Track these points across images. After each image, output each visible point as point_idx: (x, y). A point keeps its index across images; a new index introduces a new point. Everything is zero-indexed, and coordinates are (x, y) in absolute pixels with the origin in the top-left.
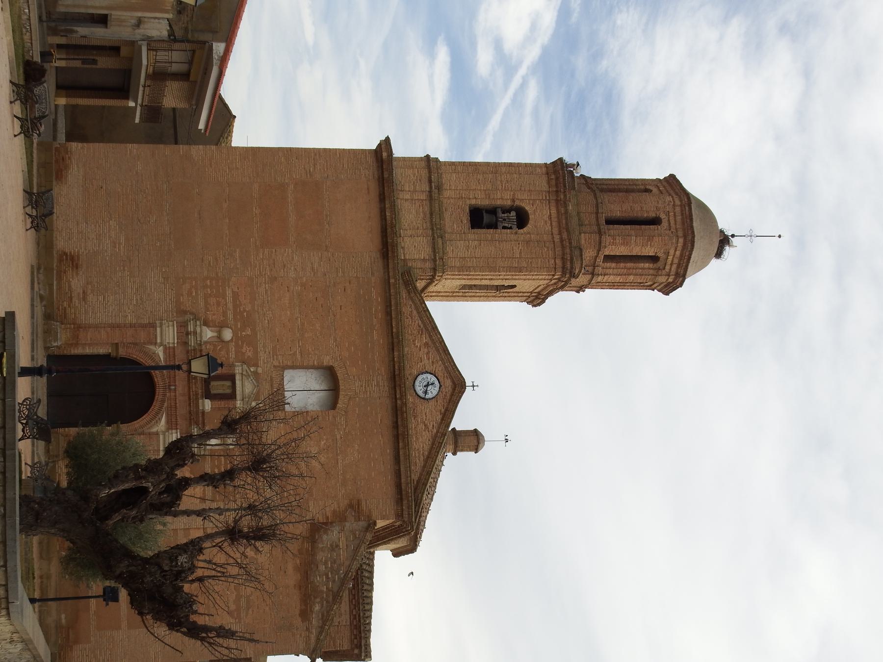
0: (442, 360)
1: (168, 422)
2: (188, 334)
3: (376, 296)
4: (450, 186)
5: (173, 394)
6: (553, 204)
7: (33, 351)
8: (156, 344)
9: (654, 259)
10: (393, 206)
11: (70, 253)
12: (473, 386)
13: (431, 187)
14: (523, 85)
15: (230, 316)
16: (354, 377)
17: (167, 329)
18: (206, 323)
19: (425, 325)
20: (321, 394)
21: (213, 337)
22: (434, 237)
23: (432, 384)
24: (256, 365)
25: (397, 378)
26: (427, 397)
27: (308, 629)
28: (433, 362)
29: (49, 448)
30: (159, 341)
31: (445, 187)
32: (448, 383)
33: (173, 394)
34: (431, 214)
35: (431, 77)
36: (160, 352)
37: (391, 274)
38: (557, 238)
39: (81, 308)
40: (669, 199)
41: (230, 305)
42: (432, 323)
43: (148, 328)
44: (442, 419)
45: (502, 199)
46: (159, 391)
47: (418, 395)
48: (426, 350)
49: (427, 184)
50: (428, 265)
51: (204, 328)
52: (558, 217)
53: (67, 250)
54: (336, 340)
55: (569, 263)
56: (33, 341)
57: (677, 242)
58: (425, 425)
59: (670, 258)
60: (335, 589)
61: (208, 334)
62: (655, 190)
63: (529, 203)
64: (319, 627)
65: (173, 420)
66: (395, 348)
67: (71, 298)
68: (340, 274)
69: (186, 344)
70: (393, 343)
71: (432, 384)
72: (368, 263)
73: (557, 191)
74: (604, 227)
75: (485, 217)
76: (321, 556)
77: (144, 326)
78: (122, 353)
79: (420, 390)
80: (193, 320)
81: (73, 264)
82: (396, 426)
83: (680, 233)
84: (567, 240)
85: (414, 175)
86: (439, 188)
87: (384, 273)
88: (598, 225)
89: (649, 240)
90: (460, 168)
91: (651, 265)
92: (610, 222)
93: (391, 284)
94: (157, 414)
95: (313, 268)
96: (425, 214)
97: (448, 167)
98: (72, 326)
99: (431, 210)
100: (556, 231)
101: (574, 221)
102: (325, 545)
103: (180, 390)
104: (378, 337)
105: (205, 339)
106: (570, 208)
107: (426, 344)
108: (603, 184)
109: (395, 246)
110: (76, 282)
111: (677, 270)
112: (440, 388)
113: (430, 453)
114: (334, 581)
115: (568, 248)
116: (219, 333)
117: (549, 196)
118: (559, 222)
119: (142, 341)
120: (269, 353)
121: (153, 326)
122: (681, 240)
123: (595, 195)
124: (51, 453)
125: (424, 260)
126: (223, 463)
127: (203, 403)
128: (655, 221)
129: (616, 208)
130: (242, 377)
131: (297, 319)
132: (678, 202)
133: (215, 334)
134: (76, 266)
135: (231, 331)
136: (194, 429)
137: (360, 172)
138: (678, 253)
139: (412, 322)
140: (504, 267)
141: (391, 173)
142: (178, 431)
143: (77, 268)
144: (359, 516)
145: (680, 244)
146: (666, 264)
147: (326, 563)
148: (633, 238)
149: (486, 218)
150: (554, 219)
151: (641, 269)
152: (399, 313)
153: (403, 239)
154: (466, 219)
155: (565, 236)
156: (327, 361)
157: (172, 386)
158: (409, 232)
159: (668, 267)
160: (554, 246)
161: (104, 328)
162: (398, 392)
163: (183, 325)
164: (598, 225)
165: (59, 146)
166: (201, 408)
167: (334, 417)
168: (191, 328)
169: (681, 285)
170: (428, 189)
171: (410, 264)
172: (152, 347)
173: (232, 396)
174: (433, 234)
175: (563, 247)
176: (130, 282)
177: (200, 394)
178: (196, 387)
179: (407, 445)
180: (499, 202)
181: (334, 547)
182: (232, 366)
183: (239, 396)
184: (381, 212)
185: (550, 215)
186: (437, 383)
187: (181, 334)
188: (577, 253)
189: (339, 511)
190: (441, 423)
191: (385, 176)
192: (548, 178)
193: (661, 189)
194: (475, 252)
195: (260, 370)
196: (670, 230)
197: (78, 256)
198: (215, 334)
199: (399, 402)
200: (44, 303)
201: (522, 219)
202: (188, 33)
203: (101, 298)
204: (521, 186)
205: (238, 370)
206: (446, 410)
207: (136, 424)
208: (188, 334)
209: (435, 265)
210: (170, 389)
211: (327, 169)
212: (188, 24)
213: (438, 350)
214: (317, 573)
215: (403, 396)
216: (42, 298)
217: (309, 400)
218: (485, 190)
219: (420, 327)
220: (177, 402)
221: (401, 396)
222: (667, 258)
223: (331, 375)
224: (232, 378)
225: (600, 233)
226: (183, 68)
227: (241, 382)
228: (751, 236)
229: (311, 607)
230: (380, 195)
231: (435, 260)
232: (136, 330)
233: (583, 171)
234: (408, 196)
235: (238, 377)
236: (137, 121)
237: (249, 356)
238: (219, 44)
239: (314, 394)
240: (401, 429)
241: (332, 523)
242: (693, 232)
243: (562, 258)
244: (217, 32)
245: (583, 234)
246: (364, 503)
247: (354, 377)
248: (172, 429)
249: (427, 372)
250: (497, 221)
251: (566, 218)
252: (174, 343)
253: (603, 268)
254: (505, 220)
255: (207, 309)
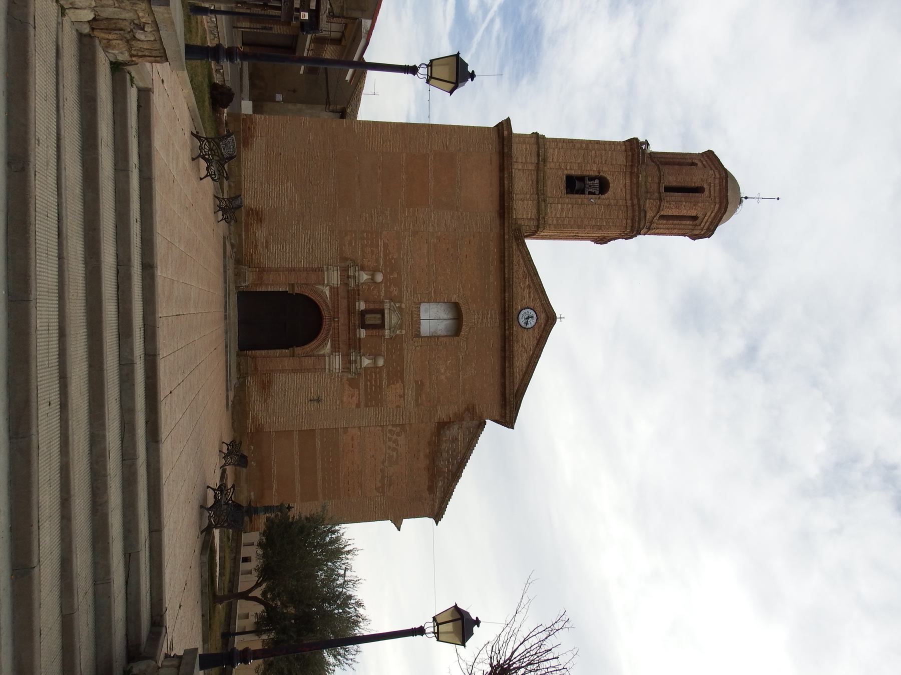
0: (539, 298)
1: (333, 346)
2: (348, 277)
3: (493, 247)
4: (553, 158)
5: (336, 324)
6: (628, 175)
7: (226, 311)
8: (323, 284)
9: (695, 218)
10: (511, 177)
11: (256, 208)
12: (561, 318)
13: (538, 160)
14: (492, 21)
15: (381, 262)
16: (474, 312)
17: (333, 272)
18: (363, 268)
19: (528, 271)
20: (448, 322)
21: (368, 279)
22: (539, 201)
23: (532, 317)
24: (401, 302)
25: (507, 314)
26: (528, 327)
27: (433, 499)
28: (532, 300)
29: (240, 368)
30: (326, 282)
31: (548, 160)
32: (543, 316)
33: (336, 324)
34: (537, 182)
35: (444, 11)
36: (327, 291)
37: (506, 231)
38: (629, 202)
39: (264, 255)
40: (711, 172)
41: (381, 254)
42: (531, 262)
43: (317, 272)
44: (537, 344)
45: (591, 170)
46: (326, 321)
47: (521, 326)
48: (528, 291)
49: (536, 158)
50: (534, 223)
51: (362, 272)
52: (631, 186)
53: (253, 207)
54: (462, 282)
55: (637, 224)
56: (226, 302)
57: (715, 207)
58: (524, 348)
59: (706, 218)
60: (454, 470)
61: (364, 277)
62: (699, 164)
63: (610, 174)
64: (441, 498)
65: (337, 345)
66: (506, 291)
67: (256, 246)
68: (467, 230)
69: (347, 285)
70: (504, 286)
71: (532, 317)
72: (488, 221)
73: (632, 166)
74: (664, 194)
75: (577, 185)
76: (444, 446)
77: (314, 270)
78: (297, 290)
79: (522, 321)
80: (353, 266)
81: (257, 218)
82: (504, 350)
83: (717, 200)
84: (637, 205)
85: (526, 149)
86: (545, 161)
87: (501, 229)
88: (659, 193)
89: (694, 205)
90: (561, 145)
91: (691, 223)
92: (668, 189)
93: (506, 239)
94: (324, 340)
95: (446, 225)
96: (532, 182)
97: (552, 143)
98: (258, 269)
99: (538, 178)
100: (628, 197)
101: (643, 189)
102: (447, 439)
103: (342, 321)
104: (493, 280)
105: (362, 281)
106: (641, 179)
107: (529, 286)
108: (662, 158)
109: (510, 209)
110: (261, 234)
111: (709, 226)
112: (537, 320)
113: (527, 370)
114: (453, 465)
115: (637, 211)
116: (373, 276)
117: (626, 169)
118: (631, 190)
119: (313, 282)
120: (411, 292)
121: (321, 270)
122: (717, 206)
123: (659, 168)
124: (242, 372)
125: (531, 219)
126: (374, 378)
127: (359, 331)
128: (699, 190)
129: (672, 180)
130: (390, 311)
131: (432, 265)
132: (718, 176)
133: (370, 277)
134: (260, 220)
135: (382, 274)
136: (352, 353)
137: (486, 146)
138: (713, 214)
139: (519, 268)
140: (588, 225)
141: (510, 149)
142: (340, 353)
143: (261, 222)
144: (473, 417)
145: (716, 209)
146: (702, 221)
147: (448, 452)
148: (684, 203)
149: (578, 185)
150: (628, 188)
151: (683, 225)
152: (511, 263)
153: (516, 202)
154: (563, 186)
155: (635, 202)
156: (454, 298)
157: (336, 318)
158: (520, 196)
159: (703, 224)
160: (627, 209)
161: (283, 271)
162: (507, 324)
163: (345, 270)
164: (659, 193)
165: (245, 117)
166: (358, 336)
167: (458, 342)
168: (351, 273)
169: (709, 237)
170: (536, 162)
171: (519, 222)
172: (320, 287)
173: (382, 326)
174: (538, 198)
175: (633, 211)
176: (304, 233)
177: (357, 324)
178: (354, 320)
179: (512, 366)
180: (588, 173)
181: (454, 439)
182: (382, 302)
183: (386, 327)
184: (500, 180)
185: (625, 183)
186: (535, 316)
187: (344, 277)
188: (642, 215)
189: (459, 414)
190: (536, 346)
191: (505, 151)
192: (627, 154)
193: (704, 163)
194: (568, 213)
195: (403, 306)
196: (710, 197)
197: (262, 212)
198: (370, 277)
199: (507, 332)
200: (235, 250)
201: (604, 186)
202: (344, 10)
203: (280, 247)
204: (606, 161)
205: (386, 306)
206: (541, 337)
207: (308, 348)
208: (348, 277)
209: (539, 224)
210: (334, 321)
211: (460, 143)
212: (343, 3)
213: (537, 291)
214: (441, 459)
215: (511, 328)
216: (232, 246)
217: (439, 326)
218: (579, 163)
219: (525, 272)
220: (340, 330)
221: (509, 327)
222: (704, 218)
223: (458, 313)
224: (382, 312)
225: (661, 199)
226: (338, 35)
227: (389, 315)
228: (759, 198)
229: (436, 484)
230: (500, 166)
231: (538, 220)
232: (308, 274)
233: (655, 147)
234: (520, 167)
235: (386, 312)
236: (302, 72)
237: (395, 295)
238: (367, 21)
239: (442, 322)
240: (507, 353)
241: (453, 422)
242: (727, 200)
243: (632, 219)
244: (365, 11)
245: (648, 200)
246: (477, 407)
247: (474, 312)
248: (335, 352)
249: (528, 308)
250: (585, 187)
251: (638, 187)
252: (338, 284)
253: (657, 224)
254: (590, 186)
255: (363, 257)
